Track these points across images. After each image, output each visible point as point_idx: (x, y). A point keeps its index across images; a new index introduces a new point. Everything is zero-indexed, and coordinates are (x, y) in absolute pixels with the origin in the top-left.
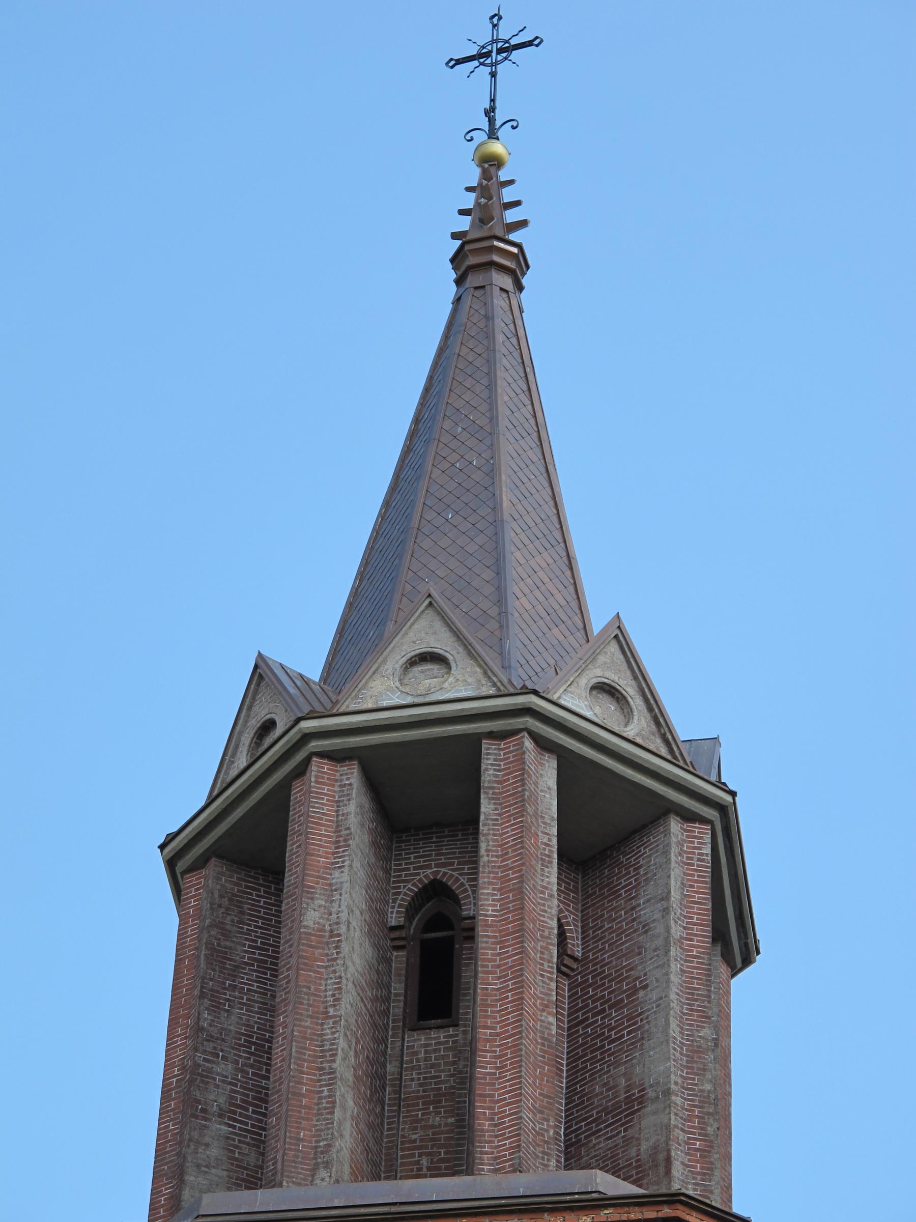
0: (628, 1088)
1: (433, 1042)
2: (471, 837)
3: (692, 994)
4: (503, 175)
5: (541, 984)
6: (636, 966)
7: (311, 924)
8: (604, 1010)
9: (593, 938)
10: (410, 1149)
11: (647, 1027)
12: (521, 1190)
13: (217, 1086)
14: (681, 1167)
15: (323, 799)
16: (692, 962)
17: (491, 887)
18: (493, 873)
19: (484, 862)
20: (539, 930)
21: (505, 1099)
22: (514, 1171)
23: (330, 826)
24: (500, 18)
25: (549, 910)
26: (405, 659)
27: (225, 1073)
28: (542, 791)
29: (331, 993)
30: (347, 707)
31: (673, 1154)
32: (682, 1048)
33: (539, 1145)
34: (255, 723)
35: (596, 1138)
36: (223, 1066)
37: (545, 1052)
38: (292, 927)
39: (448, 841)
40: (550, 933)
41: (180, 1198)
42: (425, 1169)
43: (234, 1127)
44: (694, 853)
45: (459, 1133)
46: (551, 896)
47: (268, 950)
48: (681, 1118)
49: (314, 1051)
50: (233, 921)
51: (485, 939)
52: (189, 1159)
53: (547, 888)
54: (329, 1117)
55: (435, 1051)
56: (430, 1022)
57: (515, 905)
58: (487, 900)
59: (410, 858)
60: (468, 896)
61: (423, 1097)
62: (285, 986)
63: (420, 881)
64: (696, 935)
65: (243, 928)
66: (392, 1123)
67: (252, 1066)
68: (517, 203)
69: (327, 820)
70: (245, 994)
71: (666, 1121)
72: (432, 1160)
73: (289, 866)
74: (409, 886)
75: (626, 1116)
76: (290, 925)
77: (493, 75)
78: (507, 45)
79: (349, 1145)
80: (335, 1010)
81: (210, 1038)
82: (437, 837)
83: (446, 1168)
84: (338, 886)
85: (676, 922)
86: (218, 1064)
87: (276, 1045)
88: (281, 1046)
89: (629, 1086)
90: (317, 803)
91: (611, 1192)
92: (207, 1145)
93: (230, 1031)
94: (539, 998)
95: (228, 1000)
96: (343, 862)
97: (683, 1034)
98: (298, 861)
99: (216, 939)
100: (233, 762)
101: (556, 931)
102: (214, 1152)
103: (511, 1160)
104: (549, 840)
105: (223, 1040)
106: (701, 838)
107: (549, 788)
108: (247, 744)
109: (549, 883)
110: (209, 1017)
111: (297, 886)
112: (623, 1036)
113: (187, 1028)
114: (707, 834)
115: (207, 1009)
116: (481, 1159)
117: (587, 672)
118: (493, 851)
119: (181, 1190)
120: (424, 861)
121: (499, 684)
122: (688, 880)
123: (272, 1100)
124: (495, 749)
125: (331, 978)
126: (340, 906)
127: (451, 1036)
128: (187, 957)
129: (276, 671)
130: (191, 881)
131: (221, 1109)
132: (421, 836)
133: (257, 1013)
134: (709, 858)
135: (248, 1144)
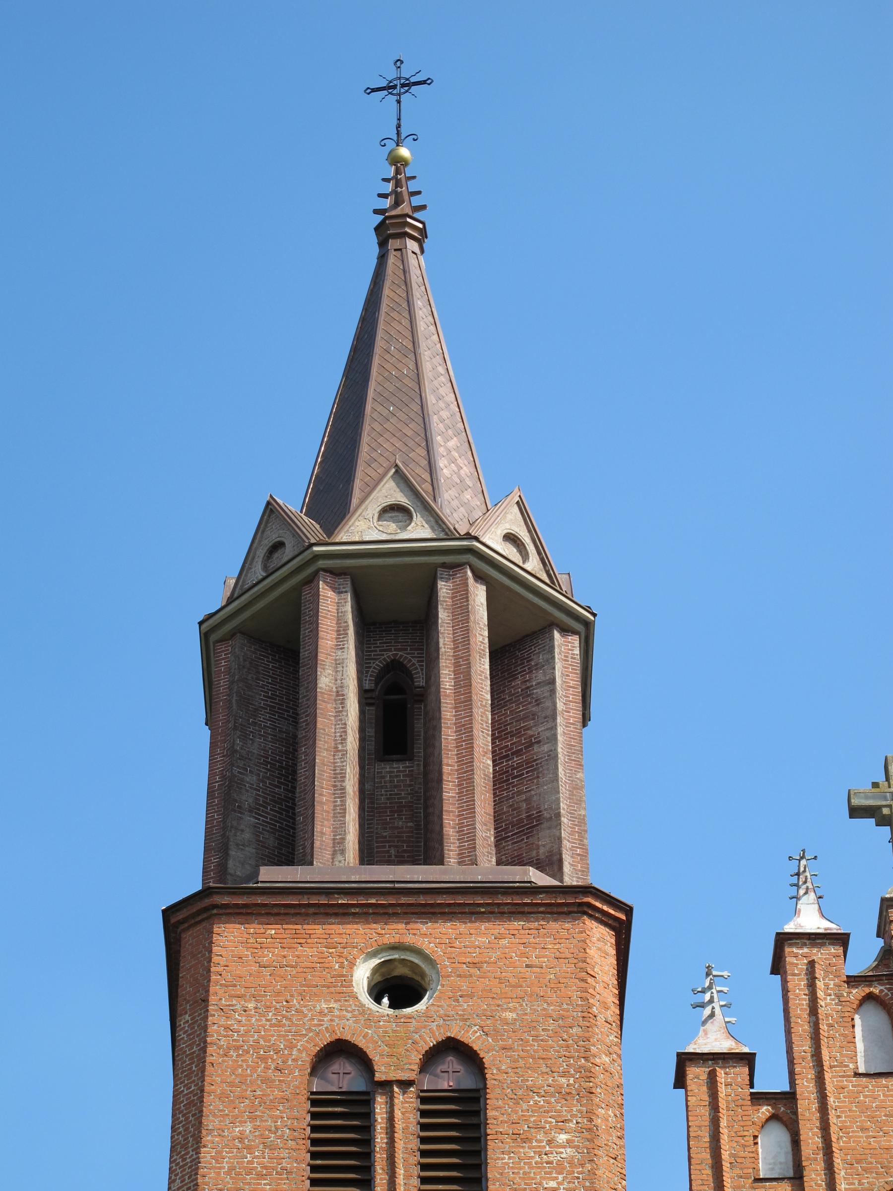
0: (528, 810)
1: (395, 770)
2: (418, 632)
3: (571, 749)
4: (409, 172)
5: (482, 737)
6: (531, 727)
7: (324, 686)
9: (497, 706)
10: (382, 842)
11: (541, 769)
12: (479, 877)
13: (247, 791)
14: (568, 866)
15: (328, 601)
16: (570, 727)
17: (448, 669)
18: (449, 660)
19: (442, 652)
20: (480, 701)
21: (463, 815)
22: (472, 864)
23: (333, 620)
24: (402, 62)
25: (485, 688)
26: (380, 508)
27: (252, 782)
28: (477, 605)
29: (339, 734)
30: (342, 538)
31: (564, 857)
32: (566, 786)
33: (485, 847)
34: (267, 543)
35: (505, 842)
36: (250, 777)
37: (486, 784)
38: (307, 687)
39: (402, 633)
40: (486, 703)
41: (226, 866)
42: (393, 856)
43: (259, 819)
44: (568, 653)
45: (417, 834)
47: (276, 699)
48: (567, 832)
49: (330, 773)
50: (252, 678)
51: (445, 705)
52: (232, 840)
53: (483, 672)
54: (342, 819)
55: (397, 776)
56: (392, 756)
57: (466, 683)
58: (445, 678)
59: (376, 644)
60: (418, 673)
61: (390, 807)
62: (304, 727)
63: (384, 659)
64: (572, 709)
65: (259, 683)
66: (371, 824)
67: (268, 778)
68: (419, 193)
69: (331, 615)
70: (262, 728)
72: (398, 851)
73: (303, 645)
74: (377, 662)
75: (527, 829)
76: (306, 685)
77: (399, 102)
78: (407, 82)
79: (352, 839)
80: (343, 747)
81: (242, 758)
82: (395, 631)
83: (408, 857)
84: (341, 661)
85: (559, 700)
86: (247, 775)
87: (300, 767)
88: (304, 768)
89: (529, 808)
90: (324, 603)
91: (540, 883)
92: (242, 831)
93: (254, 753)
94: (481, 747)
95: (252, 732)
96: (343, 645)
97: (566, 776)
98: (310, 642)
99: (242, 689)
100: (250, 568)
102: (247, 835)
103: (469, 856)
104: (483, 639)
105: (250, 759)
106: (573, 643)
107: (482, 604)
108: (262, 556)
109: (484, 669)
110: (241, 743)
111: (310, 659)
112: (523, 774)
113: (224, 749)
114: (577, 640)
115: (239, 737)
116: (448, 854)
117: (501, 525)
118: (448, 645)
119: (227, 860)
120: (387, 646)
121: (447, 530)
122: (566, 671)
123: (299, 805)
124: (446, 575)
125: (339, 724)
126: (342, 676)
127: (408, 767)
128: (221, 700)
129: (534, 548)
130: (221, 648)
131: (250, 807)
132: (384, 629)
133: (270, 742)
134: (579, 657)
135: (268, 831)
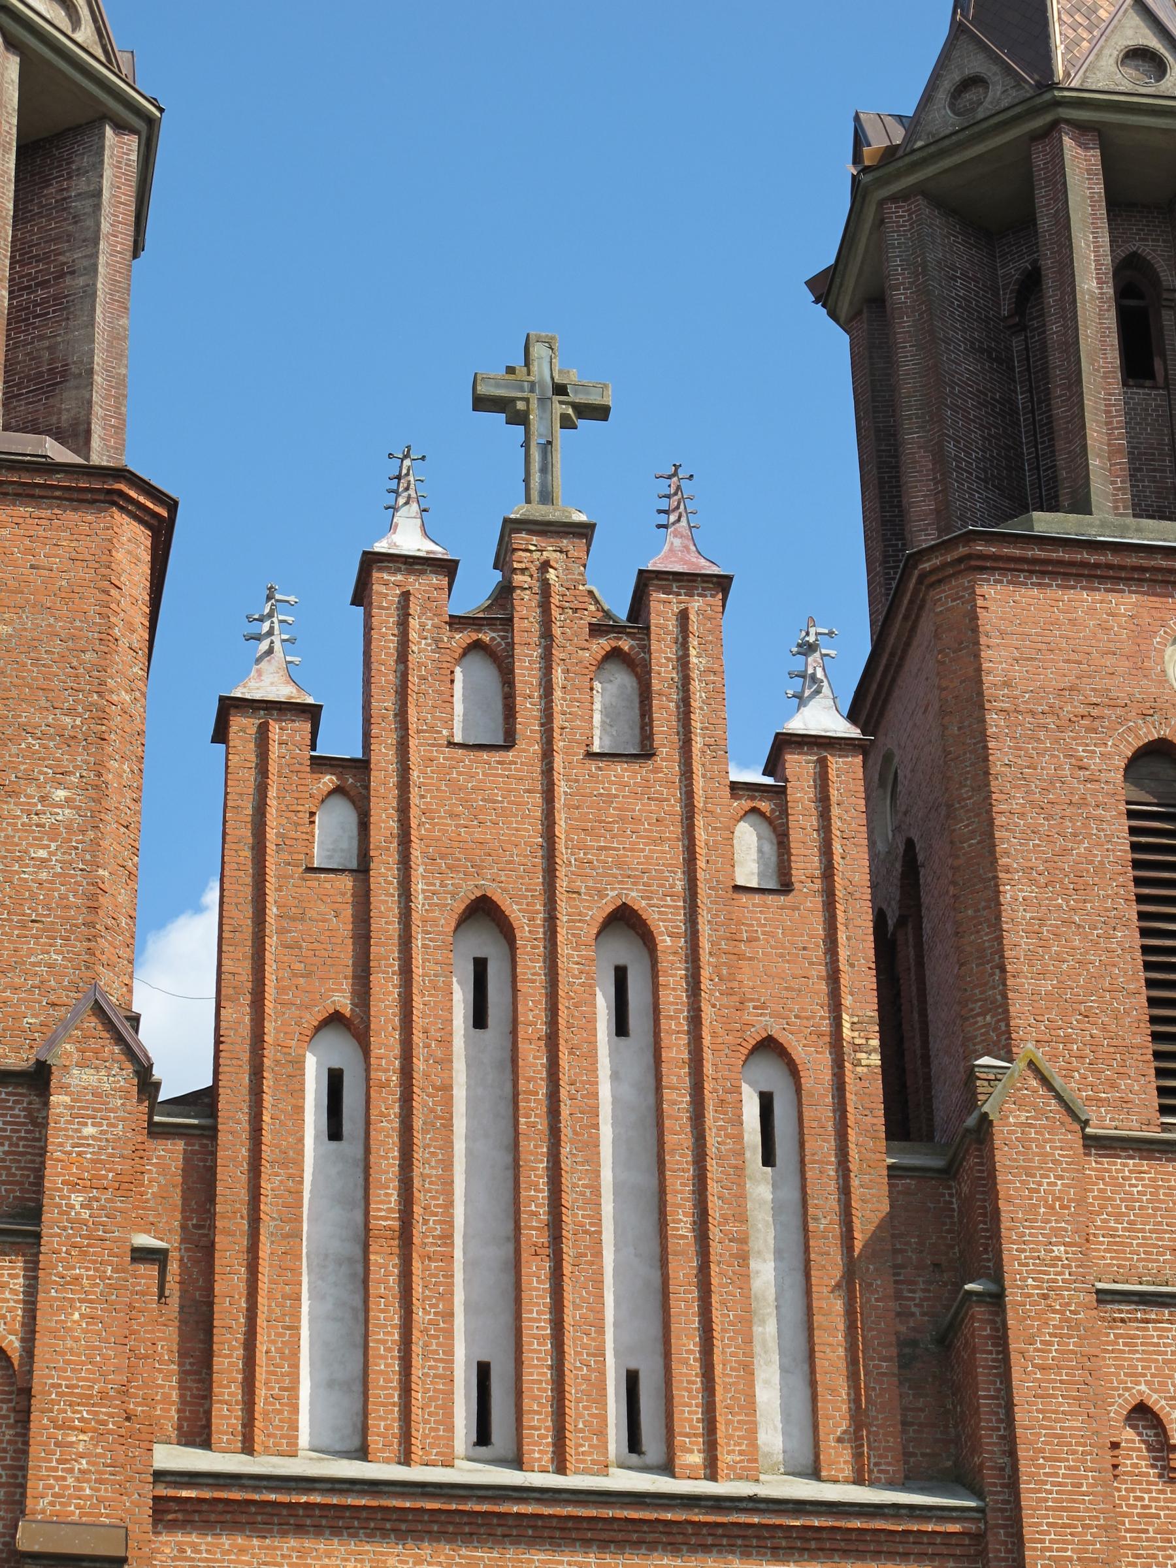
0: (52, 361)
8: (30, 287)
34: (954, 77)
46: (10, 180)
71: (88, 396)
101: (12, 213)
112: (48, 313)
